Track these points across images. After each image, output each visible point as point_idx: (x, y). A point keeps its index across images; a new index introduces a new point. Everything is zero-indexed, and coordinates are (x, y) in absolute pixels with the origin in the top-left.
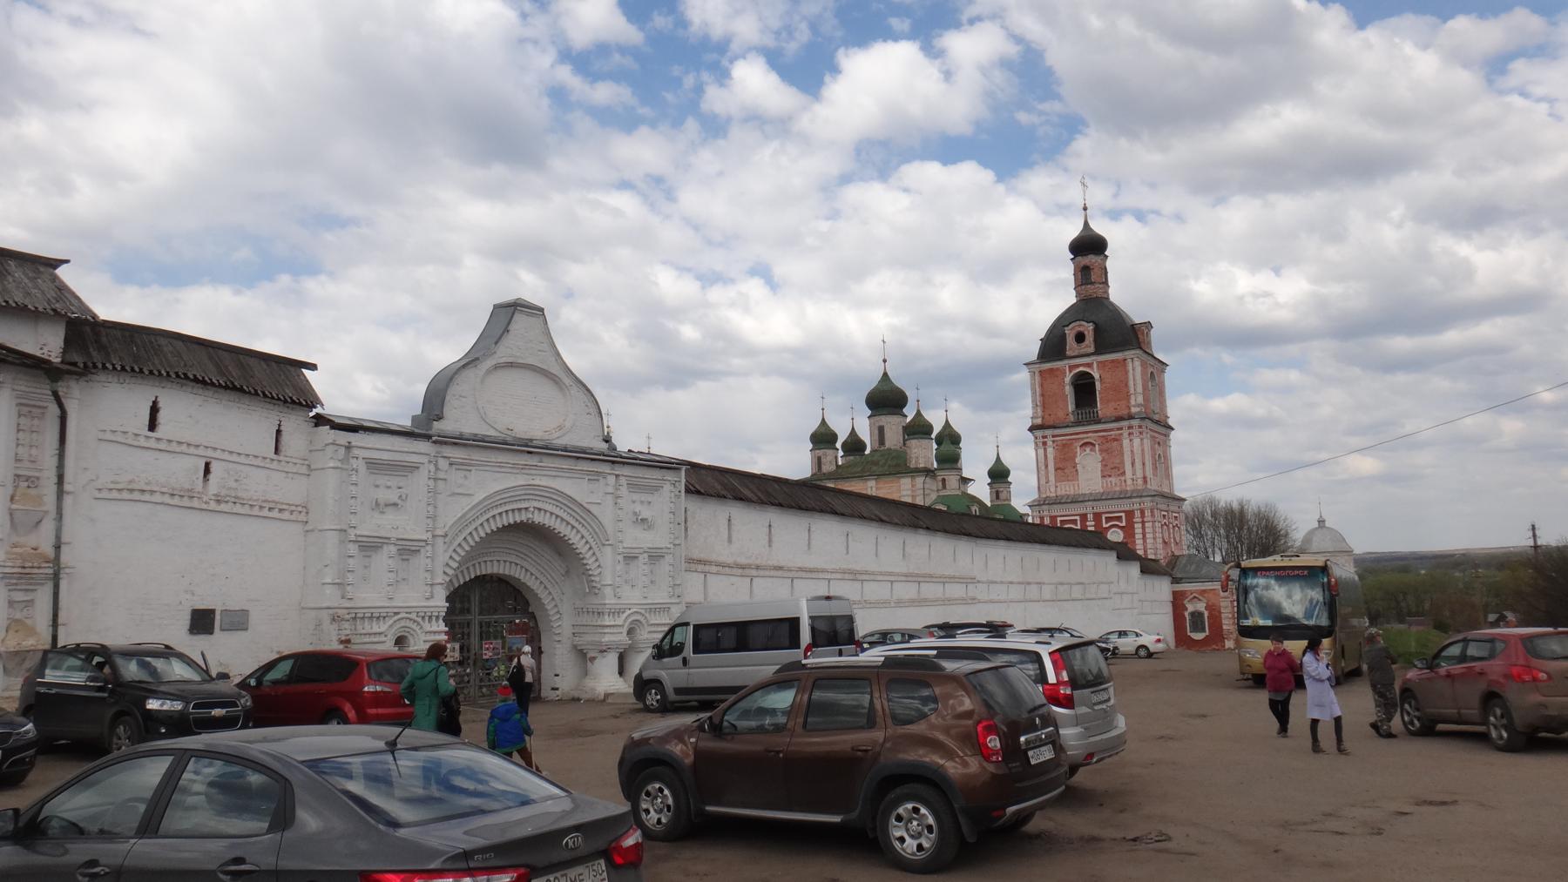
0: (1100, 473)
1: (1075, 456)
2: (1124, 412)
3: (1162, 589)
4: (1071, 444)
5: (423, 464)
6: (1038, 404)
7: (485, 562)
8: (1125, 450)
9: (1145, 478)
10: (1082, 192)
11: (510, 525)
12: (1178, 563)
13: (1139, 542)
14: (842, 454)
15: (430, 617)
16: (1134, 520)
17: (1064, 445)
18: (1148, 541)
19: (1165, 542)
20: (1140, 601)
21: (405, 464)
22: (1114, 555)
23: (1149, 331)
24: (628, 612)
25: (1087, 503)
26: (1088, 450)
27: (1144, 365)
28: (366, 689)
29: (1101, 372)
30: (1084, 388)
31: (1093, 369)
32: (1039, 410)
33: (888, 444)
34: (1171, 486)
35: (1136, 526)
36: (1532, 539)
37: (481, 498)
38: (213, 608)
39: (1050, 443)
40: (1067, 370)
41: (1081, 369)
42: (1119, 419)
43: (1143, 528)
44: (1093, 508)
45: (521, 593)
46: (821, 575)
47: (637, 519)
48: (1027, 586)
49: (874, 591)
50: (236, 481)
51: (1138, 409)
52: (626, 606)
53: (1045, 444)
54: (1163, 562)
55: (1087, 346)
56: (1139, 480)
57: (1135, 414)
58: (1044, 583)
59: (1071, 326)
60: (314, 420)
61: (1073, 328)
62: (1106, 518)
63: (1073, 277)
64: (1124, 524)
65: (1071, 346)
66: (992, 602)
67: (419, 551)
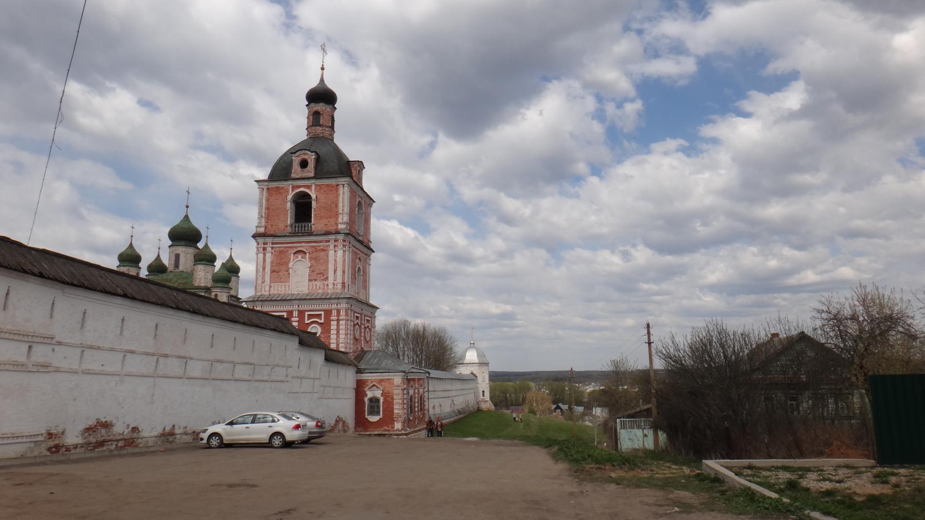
0: (308, 277)
1: (289, 262)
2: (332, 228)
3: (347, 377)
4: (287, 251)
6: (263, 215)
8: (330, 259)
9: (343, 283)
12: (365, 357)
13: (333, 337)
17: (281, 252)
19: (355, 339)
20: (322, 386)
22: (296, 340)
25: (293, 302)
26: (300, 257)
27: (352, 192)
29: (318, 193)
30: (303, 207)
31: (311, 190)
32: (263, 220)
33: (181, 268)
34: (367, 295)
35: (332, 323)
39: (269, 249)
41: (302, 189)
42: (327, 233)
43: (338, 325)
44: (298, 307)
48: (162, 360)
53: (264, 249)
54: (352, 356)
55: (308, 172)
57: (342, 229)
58: (191, 359)
59: (297, 154)
62: (308, 315)
63: (306, 120)
64: (322, 321)
65: (296, 171)
66: (87, 372)
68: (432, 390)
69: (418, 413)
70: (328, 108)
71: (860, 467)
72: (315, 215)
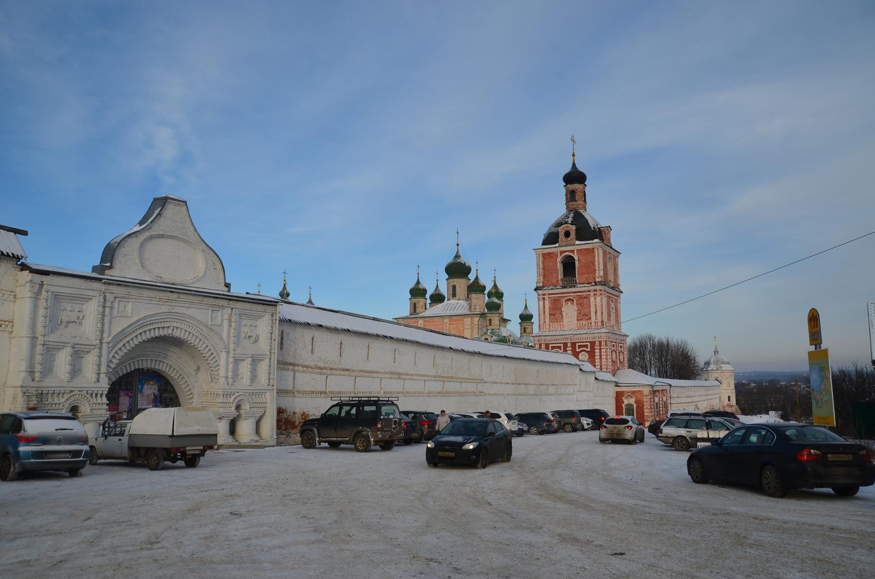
4: (560, 299)
5: (95, 296)
7: (142, 360)
8: (591, 304)
9: (602, 321)
11: (156, 337)
14: (430, 302)
15: (96, 395)
16: (595, 348)
17: (555, 300)
19: (613, 362)
21: (81, 296)
23: (610, 232)
24: (236, 395)
26: (569, 303)
28: (805, 458)
30: (569, 265)
31: (574, 254)
32: (541, 278)
35: (596, 351)
37: (136, 319)
41: (567, 253)
43: (600, 352)
46: (375, 375)
47: (246, 336)
49: (411, 386)
51: (600, 280)
53: (544, 299)
58: (530, 384)
60: (21, 267)
61: (563, 228)
62: (552, 347)
64: (589, 350)
67: (90, 352)
68: (676, 396)
69: (663, 415)
70: (581, 186)
71: (298, 365)
72: (578, 272)
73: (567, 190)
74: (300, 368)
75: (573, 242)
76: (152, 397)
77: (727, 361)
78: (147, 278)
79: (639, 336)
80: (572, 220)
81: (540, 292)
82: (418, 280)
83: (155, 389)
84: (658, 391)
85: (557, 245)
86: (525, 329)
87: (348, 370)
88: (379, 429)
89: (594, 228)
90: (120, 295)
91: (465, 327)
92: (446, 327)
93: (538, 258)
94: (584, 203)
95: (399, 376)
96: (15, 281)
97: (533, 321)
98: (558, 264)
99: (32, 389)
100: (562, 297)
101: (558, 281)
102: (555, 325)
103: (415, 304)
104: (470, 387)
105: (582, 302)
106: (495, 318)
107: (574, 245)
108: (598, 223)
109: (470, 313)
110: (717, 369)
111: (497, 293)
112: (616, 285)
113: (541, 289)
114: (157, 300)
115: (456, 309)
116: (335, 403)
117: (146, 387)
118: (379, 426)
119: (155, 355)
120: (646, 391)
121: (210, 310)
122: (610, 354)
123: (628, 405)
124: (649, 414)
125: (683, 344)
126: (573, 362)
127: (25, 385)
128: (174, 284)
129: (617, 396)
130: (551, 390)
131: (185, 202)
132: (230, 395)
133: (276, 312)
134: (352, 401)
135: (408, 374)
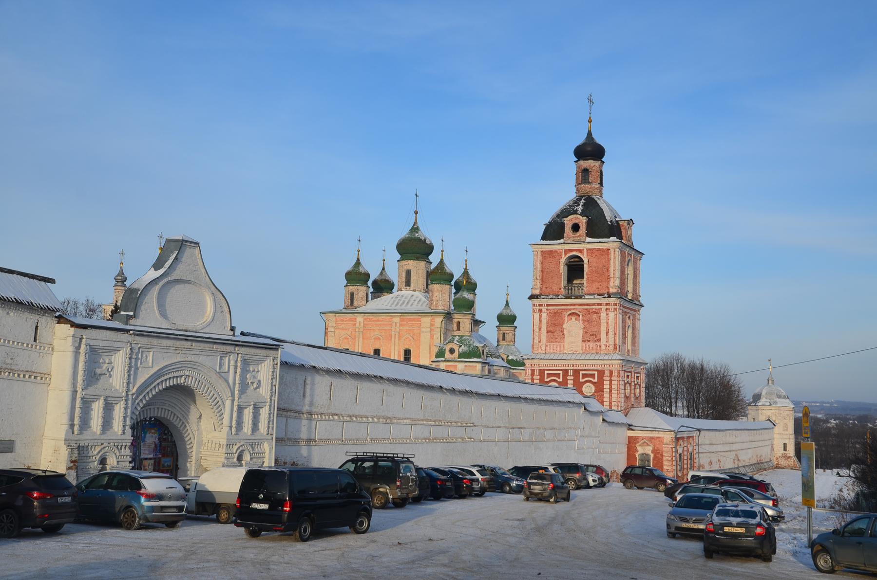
6: (538, 278)
9: (615, 345)
10: (589, 108)
17: (555, 313)
18: (613, 395)
21: (112, 348)
24: (238, 445)
26: (574, 319)
30: (575, 269)
31: (583, 254)
36: (700, 456)
38: (713, 564)
40: (563, 248)
41: (574, 253)
43: (611, 384)
45: (168, 428)
46: (363, 420)
50: (12, 359)
52: (237, 441)
53: (540, 311)
56: (611, 347)
58: (524, 428)
61: (571, 220)
64: (596, 380)
68: (708, 442)
73: (578, 167)
74: (293, 414)
75: (583, 239)
76: (153, 446)
77: (784, 393)
78: (163, 324)
79: (663, 355)
80: (582, 209)
81: (536, 301)
82: (358, 259)
83: (156, 437)
84: (683, 438)
85: (562, 241)
86: (504, 334)
87: (337, 415)
88: (398, 487)
89: (611, 221)
90: (144, 345)
91: (423, 330)
92: (395, 329)
93: (536, 255)
94: (599, 185)
95: (386, 420)
96: (53, 334)
97: (516, 324)
98: (562, 267)
99: (73, 442)
100: (565, 309)
101: (560, 289)
102: (554, 347)
103: (352, 294)
104: (459, 432)
105: (590, 317)
106: (465, 320)
107: (584, 242)
108: (617, 213)
109: (429, 310)
110: (770, 405)
111: (466, 284)
112: (635, 296)
113: (537, 298)
114: (174, 348)
115: (411, 303)
116: (350, 458)
117: (148, 435)
118: (398, 484)
119: (161, 403)
120: (668, 437)
121: (219, 357)
122: (623, 386)
123: (643, 454)
124: (670, 468)
125: (722, 370)
126: (577, 401)
127: (67, 438)
128: (186, 331)
129: (629, 442)
130: (549, 435)
131: (198, 244)
132: (233, 445)
133: (277, 356)
134: (366, 455)
135: (395, 418)
